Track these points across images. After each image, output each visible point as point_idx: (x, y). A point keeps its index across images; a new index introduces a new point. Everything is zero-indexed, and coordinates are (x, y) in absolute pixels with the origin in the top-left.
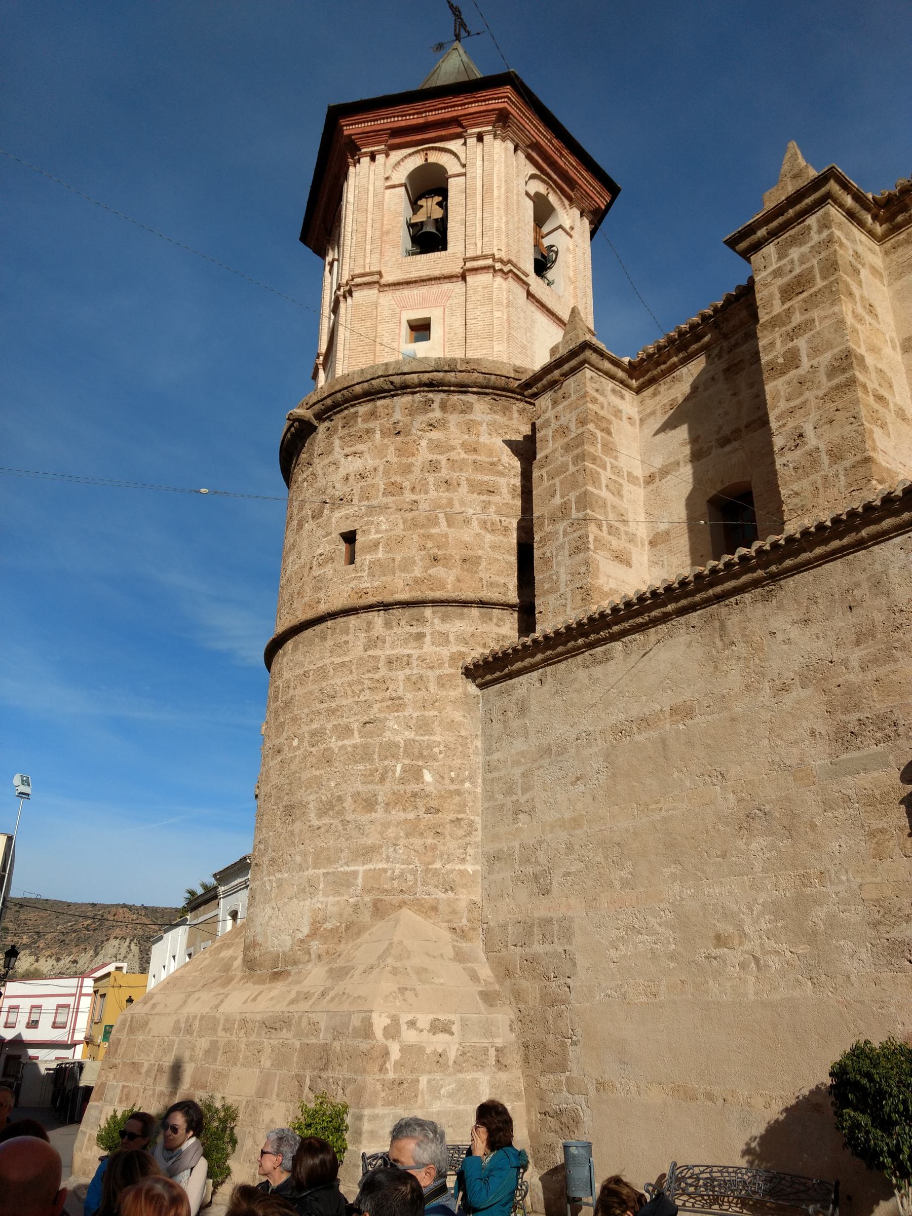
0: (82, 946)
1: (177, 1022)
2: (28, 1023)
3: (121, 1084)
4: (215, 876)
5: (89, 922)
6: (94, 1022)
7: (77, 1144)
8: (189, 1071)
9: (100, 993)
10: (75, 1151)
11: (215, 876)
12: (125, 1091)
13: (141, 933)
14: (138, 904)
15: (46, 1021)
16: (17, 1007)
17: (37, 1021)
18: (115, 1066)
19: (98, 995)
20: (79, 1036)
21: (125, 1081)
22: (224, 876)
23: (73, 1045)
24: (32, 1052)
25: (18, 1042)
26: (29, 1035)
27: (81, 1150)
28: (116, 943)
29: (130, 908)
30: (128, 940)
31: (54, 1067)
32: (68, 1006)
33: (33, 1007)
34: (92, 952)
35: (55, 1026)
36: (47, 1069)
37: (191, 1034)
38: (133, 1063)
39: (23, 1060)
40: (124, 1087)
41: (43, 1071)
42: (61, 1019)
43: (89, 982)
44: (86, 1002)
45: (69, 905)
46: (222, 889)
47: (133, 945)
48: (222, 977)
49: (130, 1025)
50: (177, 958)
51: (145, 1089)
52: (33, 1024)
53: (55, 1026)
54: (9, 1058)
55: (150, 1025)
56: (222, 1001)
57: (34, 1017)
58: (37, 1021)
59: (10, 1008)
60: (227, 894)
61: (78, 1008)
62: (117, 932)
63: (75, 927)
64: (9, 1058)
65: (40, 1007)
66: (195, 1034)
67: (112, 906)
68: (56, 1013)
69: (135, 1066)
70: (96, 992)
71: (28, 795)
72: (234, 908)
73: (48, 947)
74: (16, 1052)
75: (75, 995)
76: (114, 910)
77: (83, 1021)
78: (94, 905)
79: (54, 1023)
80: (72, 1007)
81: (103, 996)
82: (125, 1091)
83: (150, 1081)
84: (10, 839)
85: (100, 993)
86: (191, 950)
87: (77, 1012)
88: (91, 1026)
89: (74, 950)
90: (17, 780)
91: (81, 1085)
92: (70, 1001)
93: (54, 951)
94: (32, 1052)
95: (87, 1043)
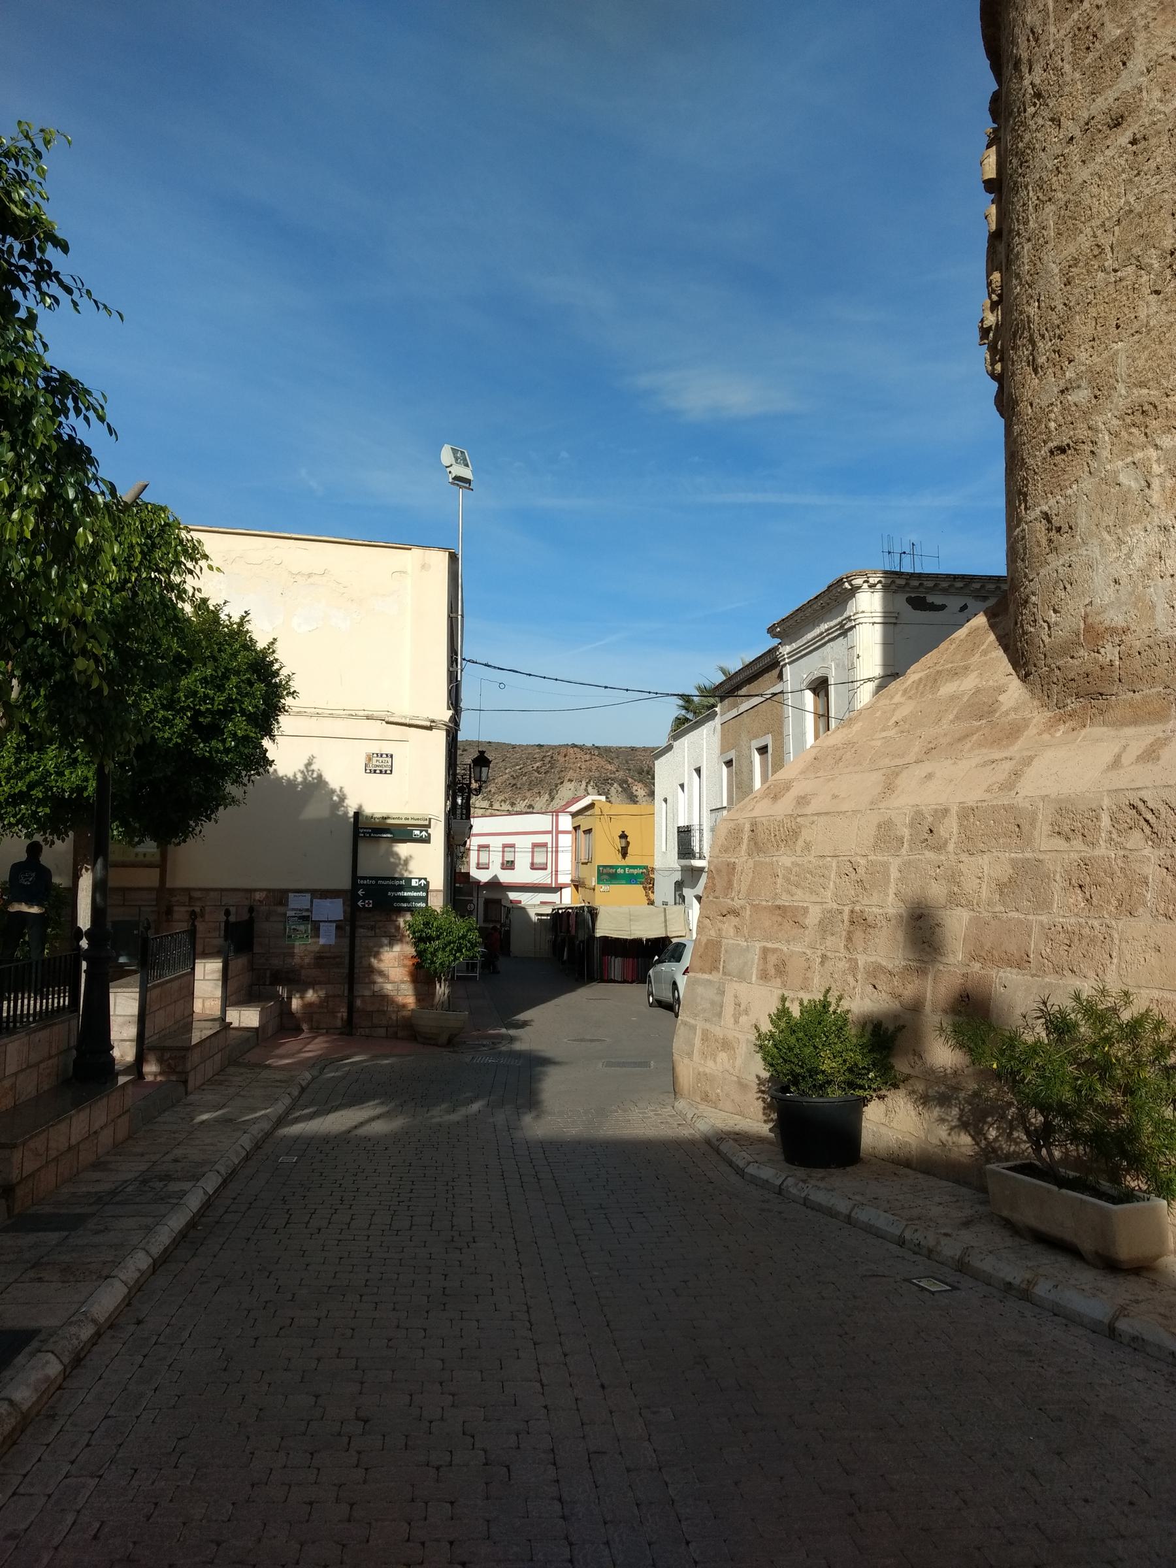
0: (536, 790)
1: (885, 827)
2: (503, 864)
3: (758, 945)
4: (771, 630)
5: (538, 764)
6: (581, 862)
7: (678, 1044)
8: (957, 925)
9: (583, 828)
10: (676, 1057)
11: (771, 630)
12: (773, 959)
13: (597, 774)
14: (589, 744)
15: (523, 861)
16: (488, 846)
17: (513, 862)
18: (735, 912)
19: (580, 832)
20: (564, 879)
21: (767, 939)
22: (788, 628)
23: (559, 889)
24: (513, 896)
25: (494, 884)
26: (506, 877)
27: (690, 1055)
28: (571, 786)
29: (581, 748)
30: (584, 783)
31: (550, 912)
32: (545, 845)
33: (504, 846)
34: (547, 796)
35: (533, 867)
36: (538, 914)
37: (940, 848)
38: (779, 907)
39: (504, 903)
40: (765, 951)
41: (535, 918)
42: (540, 859)
43: (566, 822)
44: (566, 841)
45: (514, 747)
46: (786, 650)
47: (590, 788)
48: (979, 729)
49: (751, 839)
50: (704, 772)
51: (824, 957)
52: (509, 865)
53: (533, 867)
54: (488, 902)
55: (805, 835)
56: (1017, 774)
57: (509, 857)
58: (513, 862)
59: (480, 847)
60: (797, 657)
61: (557, 847)
62: (570, 774)
63: (524, 770)
64: (488, 902)
65: (513, 846)
66: (951, 847)
67: (561, 746)
68: (533, 852)
69: (790, 916)
70: (576, 828)
71: (468, 481)
72: (817, 674)
73: (500, 791)
74: (496, 896)
75: (550, 832)
76: (563, 751)
77: (566, 862)
78: (540, 746)
79: (532, 864)
80: (549, 845)
81: (588, 831)
82: (773, 959)
83: (835, 942)
84: (453, 558)
85: (583, 828)
86: (732, 754)
87: (557, 852)
88: (577, 868)
89: (528, 794)
90: (446, 456)
91: (598, 935)
92: (546, 839)
93: (507, 795)
94: (513, 896)
95: (576, 887)
